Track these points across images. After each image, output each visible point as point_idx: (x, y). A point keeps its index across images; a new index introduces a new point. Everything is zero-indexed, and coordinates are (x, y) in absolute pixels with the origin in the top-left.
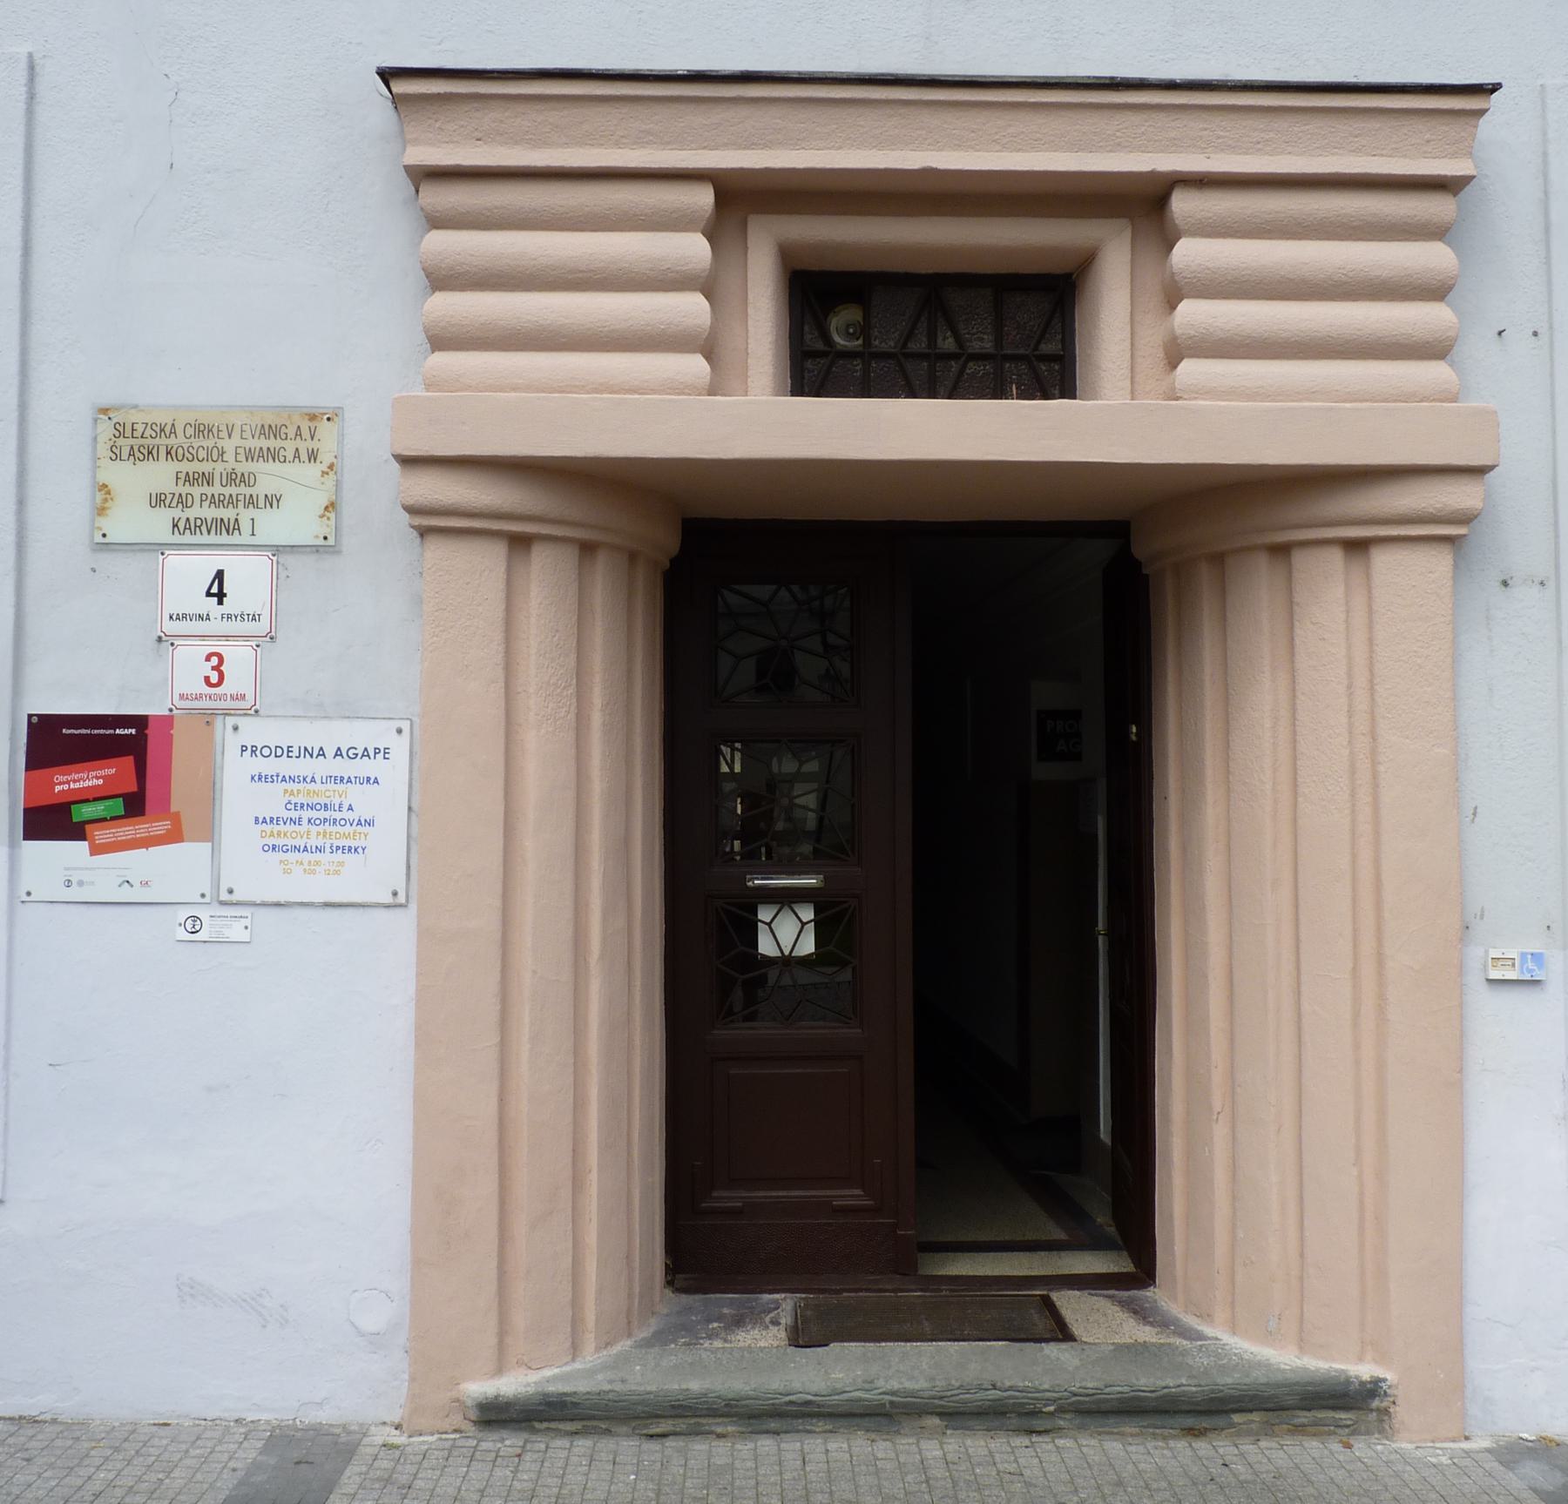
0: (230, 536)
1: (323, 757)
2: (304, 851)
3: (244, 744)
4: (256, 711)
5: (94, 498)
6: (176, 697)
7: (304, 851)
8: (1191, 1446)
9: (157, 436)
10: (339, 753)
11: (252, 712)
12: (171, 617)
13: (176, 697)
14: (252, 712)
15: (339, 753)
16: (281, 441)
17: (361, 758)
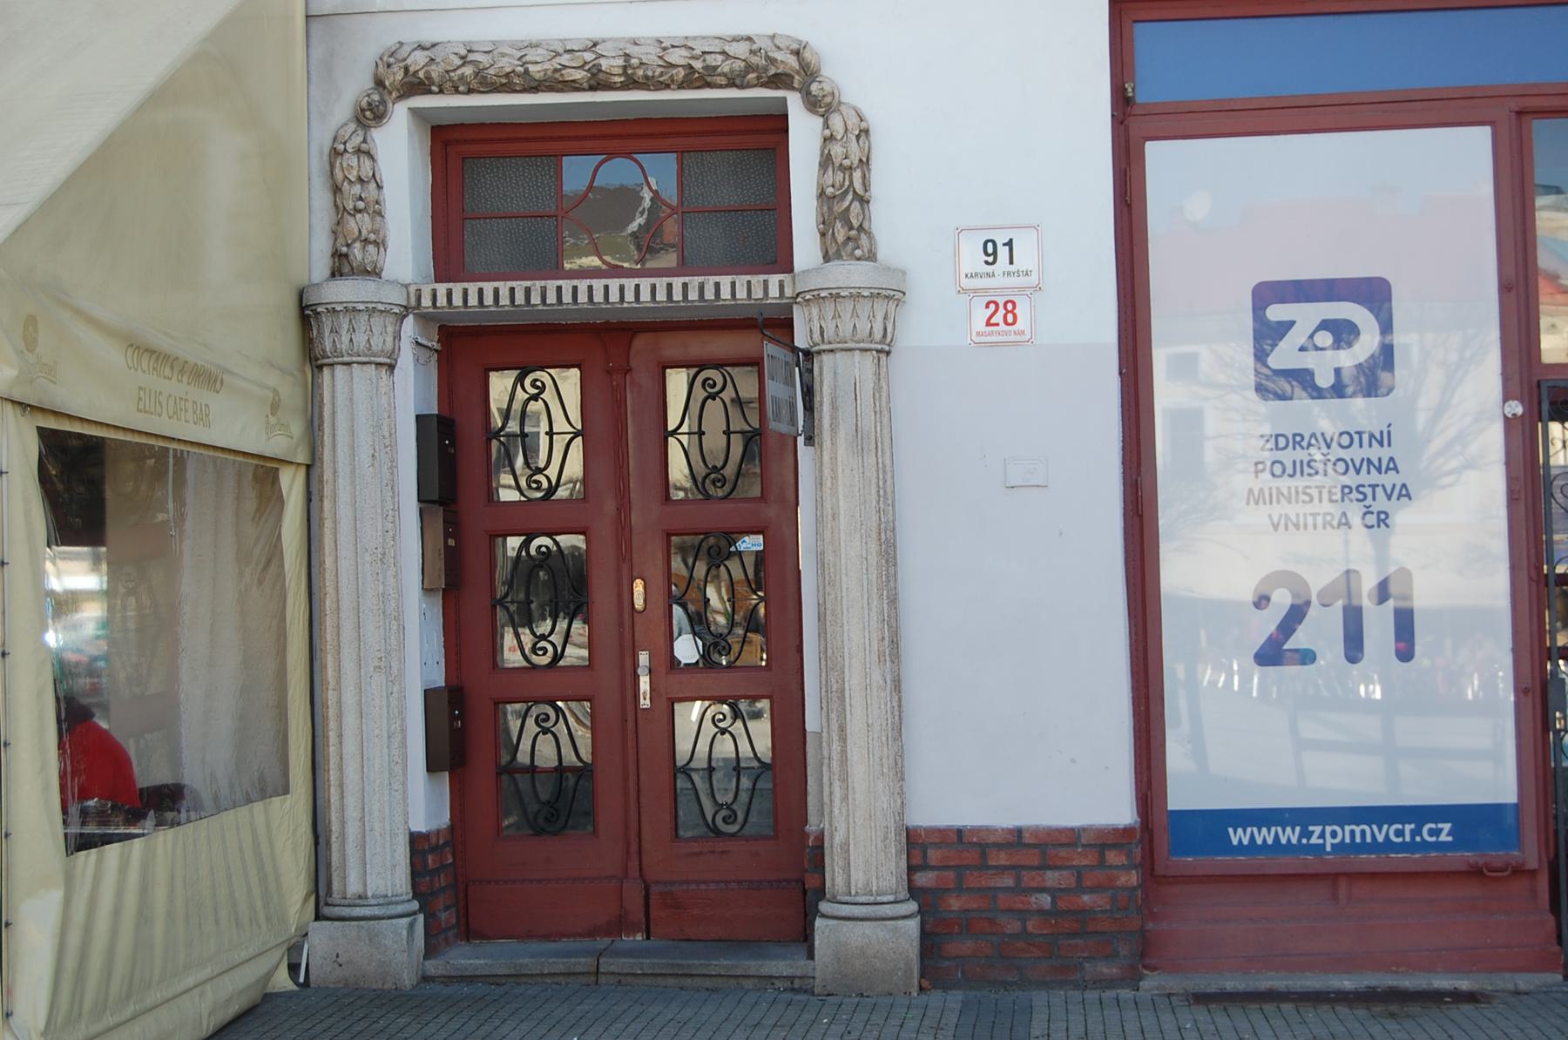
0: (1365, 457)
1: (1394, 472)
2: (1388, 469)
3: (1297, 432)
4: (1040, 288)
5: (674, 90)
6: (974, 334)
7: (1388, 469)
8: (1333, 1009)
9: (1287, 446)
10: (1404, 492)
11: (1037, 289)
12: (967, 276)
13: (974, 334)
14: (1037, 289)
15: (1404, 492)
16: (1301, 451)
17: (1398, 499)
